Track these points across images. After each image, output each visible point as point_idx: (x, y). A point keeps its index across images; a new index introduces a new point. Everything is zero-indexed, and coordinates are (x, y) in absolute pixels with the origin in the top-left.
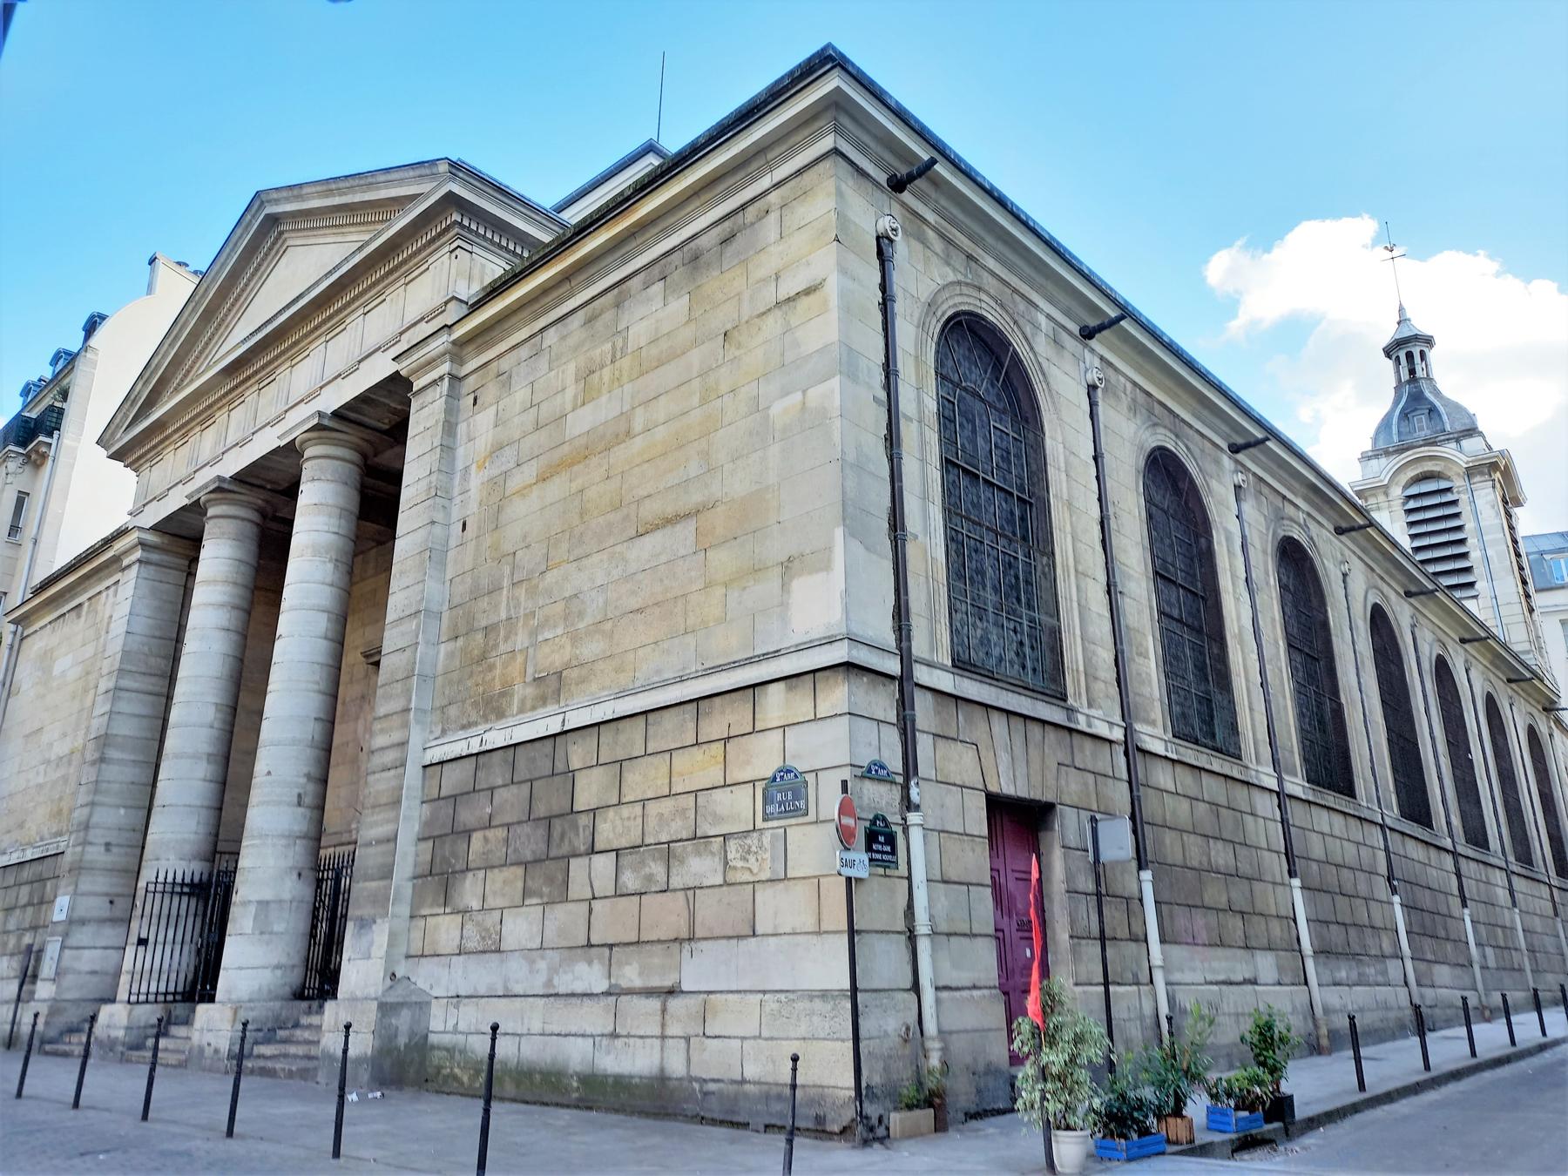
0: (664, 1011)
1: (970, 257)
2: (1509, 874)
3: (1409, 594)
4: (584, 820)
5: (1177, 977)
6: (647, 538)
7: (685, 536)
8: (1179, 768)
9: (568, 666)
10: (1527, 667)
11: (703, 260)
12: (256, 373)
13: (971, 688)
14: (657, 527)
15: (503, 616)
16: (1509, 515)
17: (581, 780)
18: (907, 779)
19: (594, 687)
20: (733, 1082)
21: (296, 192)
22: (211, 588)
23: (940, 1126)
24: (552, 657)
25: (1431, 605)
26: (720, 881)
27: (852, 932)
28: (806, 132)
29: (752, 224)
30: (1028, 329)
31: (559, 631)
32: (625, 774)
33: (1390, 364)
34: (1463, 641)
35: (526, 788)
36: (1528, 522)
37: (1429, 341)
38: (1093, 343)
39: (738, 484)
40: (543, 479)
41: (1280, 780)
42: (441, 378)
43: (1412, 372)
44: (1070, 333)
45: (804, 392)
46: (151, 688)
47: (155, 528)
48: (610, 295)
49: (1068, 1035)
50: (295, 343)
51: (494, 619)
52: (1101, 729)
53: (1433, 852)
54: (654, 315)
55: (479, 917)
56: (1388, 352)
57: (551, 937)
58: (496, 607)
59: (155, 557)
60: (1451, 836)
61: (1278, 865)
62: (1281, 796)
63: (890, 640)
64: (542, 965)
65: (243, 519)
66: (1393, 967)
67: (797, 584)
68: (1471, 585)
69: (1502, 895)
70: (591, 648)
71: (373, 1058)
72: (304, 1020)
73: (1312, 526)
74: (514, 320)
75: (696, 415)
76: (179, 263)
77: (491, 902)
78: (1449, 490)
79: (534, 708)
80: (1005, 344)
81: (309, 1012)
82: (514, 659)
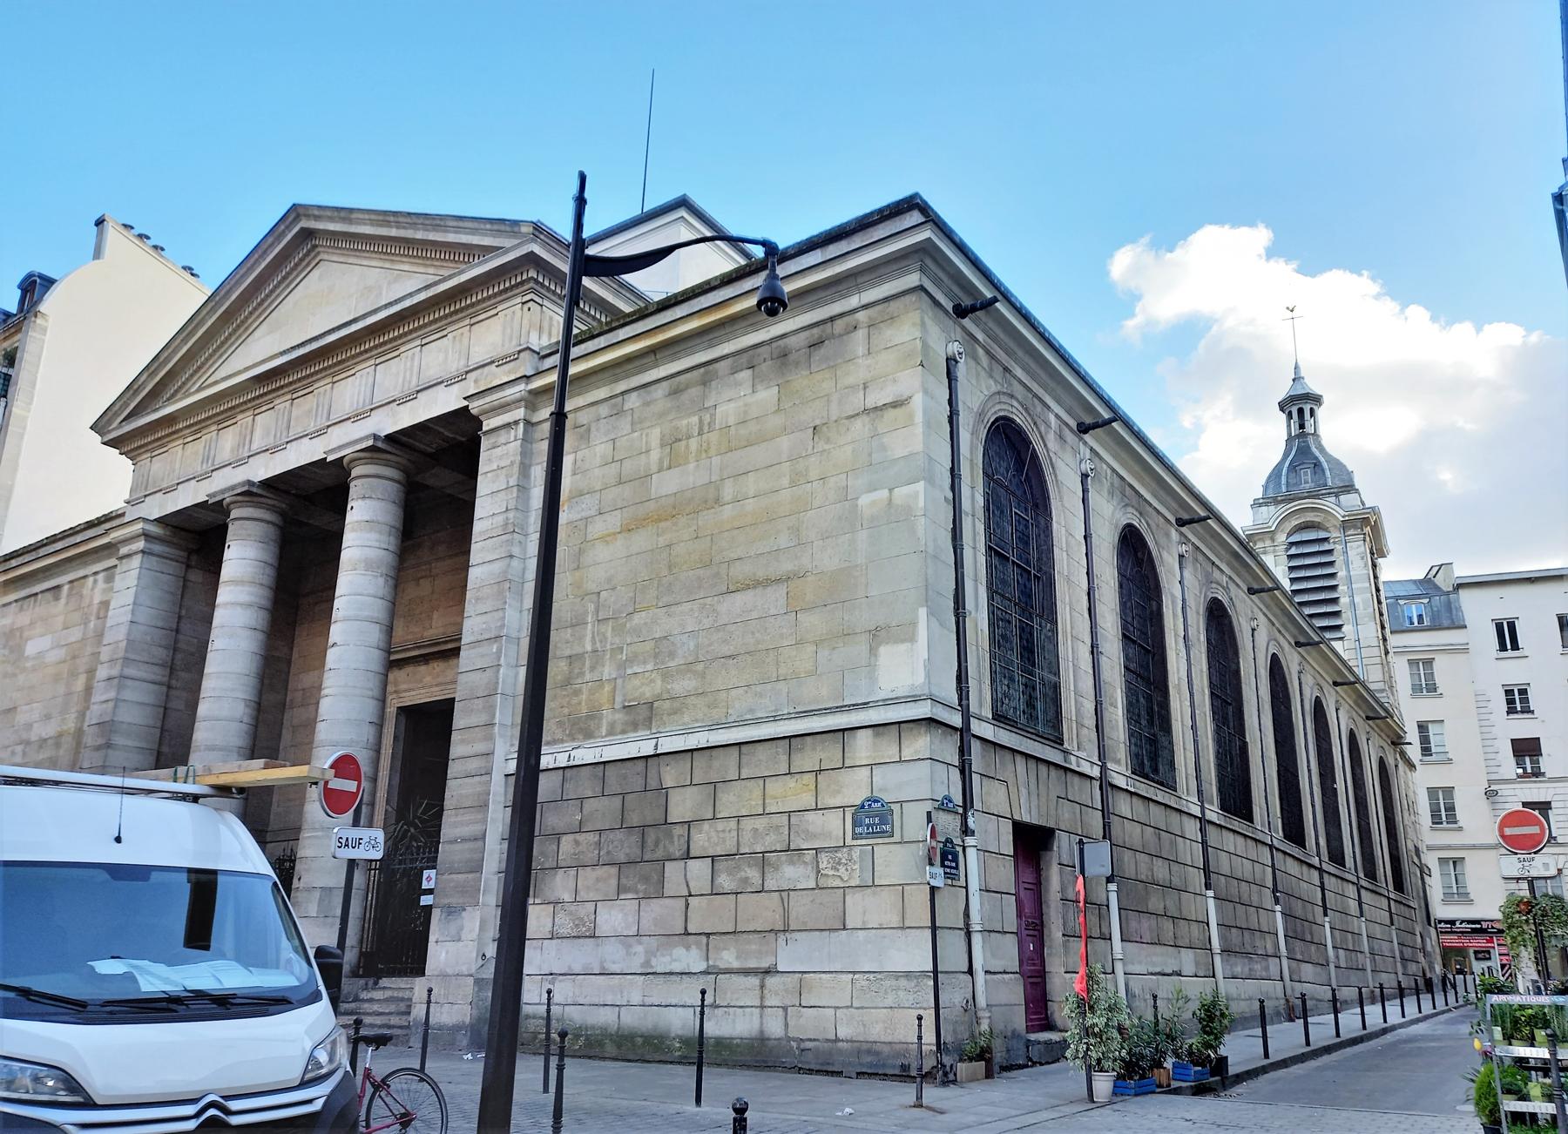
0: (762, 987)
1: (1006, 369)
2: (1359, 888)
3: (1298, 644)
4: (679, 831)
5: (1130, 969)
6: (738, 596)
7: (765, 591)
8: (1135, 799)
9: (659, 698)
10: (1381, 705)
11: (792, 357)
12: (291, 383)
13: (1005, 737)
14: (748, 587)
15: (589, 648)
16: (1374, 566)
17: (675, 798)
18: (965, 807)
19: (686, 719)
20: (828, 1040)
21: (343, 214)
22: (240, 588)
23: (989, 1075)
24: (645, 686)
25: (1314, 653)
26: (813, 885)
27: (934, 929)
28: (895, 267)
29: (841, 335)
30: (1043, 429)
31: (649, 667)
32: (719, 795)
33: (1283, 417)
34: (1336, 684)
35: (617, 801)
36: (1391, 571)
37: (1317, 400)
38: (1087, 437)
39: (827, 559)
40: (627, 529)
41: (1202, 807)
42: (516, 422)
43: (1302, 426)
44: (1071, 429)
45: (891, 490)
46: (153, 677)
47: (160, 521)
48: (695, 373)
49: (1103, 1005)
50: (340, 363)
51: (577, 650)
52: (1086, 768)
53: (1305, 868)
54: (740, 400)
55: (573, 908)
56: (1282, 406)
57: (647, 926)
58: (581, 638)
59: (157, 548)
60: (1319, 855)
61: (1197, 878)
62: (1203, 821)
63: (953, 698)
64: (640, 949)
65: (268, 522)
66: (1273, 962)
67: (883, 650)
68: (1338, 628)
69: (1353, 906)
70: (683, 685)
71: (472, 1026)
72: (364, 995)
73: (1232, 587)
74: (593, 379)
75: (785, 495)
76: (125, 226)
77: (583, 895)
78: (1326, 540)
79: (623, 732)
80: (1027, 442)
81: (366, 988)
82: (602, 687)
